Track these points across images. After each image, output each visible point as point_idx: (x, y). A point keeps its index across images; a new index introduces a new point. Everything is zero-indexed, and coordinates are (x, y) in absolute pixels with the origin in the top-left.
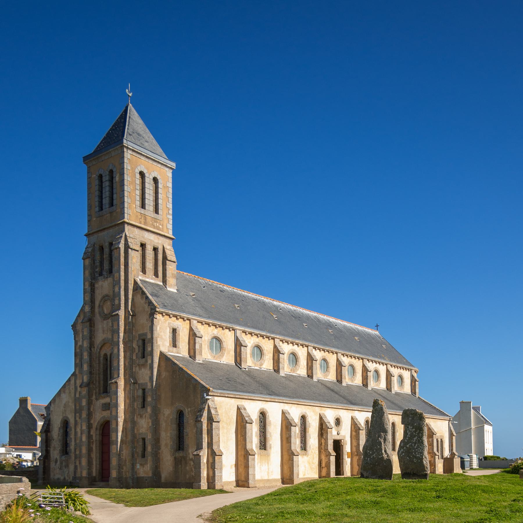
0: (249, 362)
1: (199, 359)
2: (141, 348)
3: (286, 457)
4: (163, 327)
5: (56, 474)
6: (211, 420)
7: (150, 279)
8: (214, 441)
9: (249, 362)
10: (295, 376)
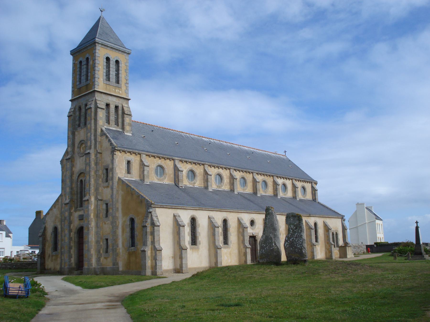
0: (185, 182)
1: (147, 181)
2: (105, 175)
3: (213, 251)
4: (120, 161)
5: (50, 264)
6: (153, 224)
7: (113, 128)
8: (155, 240)
9: (185, 182)
10: (221, 191)
